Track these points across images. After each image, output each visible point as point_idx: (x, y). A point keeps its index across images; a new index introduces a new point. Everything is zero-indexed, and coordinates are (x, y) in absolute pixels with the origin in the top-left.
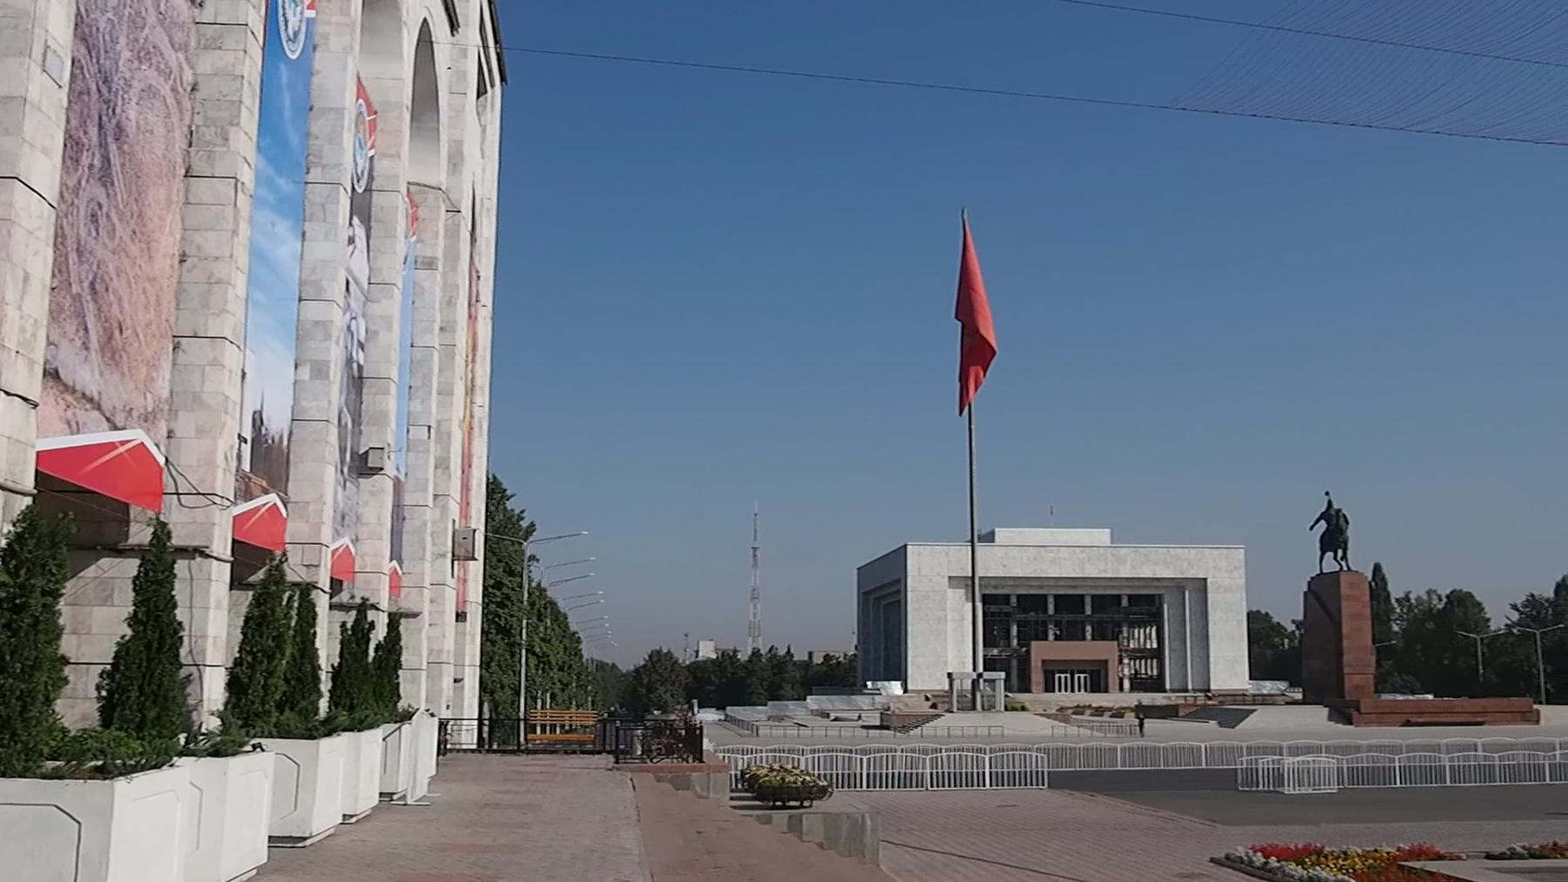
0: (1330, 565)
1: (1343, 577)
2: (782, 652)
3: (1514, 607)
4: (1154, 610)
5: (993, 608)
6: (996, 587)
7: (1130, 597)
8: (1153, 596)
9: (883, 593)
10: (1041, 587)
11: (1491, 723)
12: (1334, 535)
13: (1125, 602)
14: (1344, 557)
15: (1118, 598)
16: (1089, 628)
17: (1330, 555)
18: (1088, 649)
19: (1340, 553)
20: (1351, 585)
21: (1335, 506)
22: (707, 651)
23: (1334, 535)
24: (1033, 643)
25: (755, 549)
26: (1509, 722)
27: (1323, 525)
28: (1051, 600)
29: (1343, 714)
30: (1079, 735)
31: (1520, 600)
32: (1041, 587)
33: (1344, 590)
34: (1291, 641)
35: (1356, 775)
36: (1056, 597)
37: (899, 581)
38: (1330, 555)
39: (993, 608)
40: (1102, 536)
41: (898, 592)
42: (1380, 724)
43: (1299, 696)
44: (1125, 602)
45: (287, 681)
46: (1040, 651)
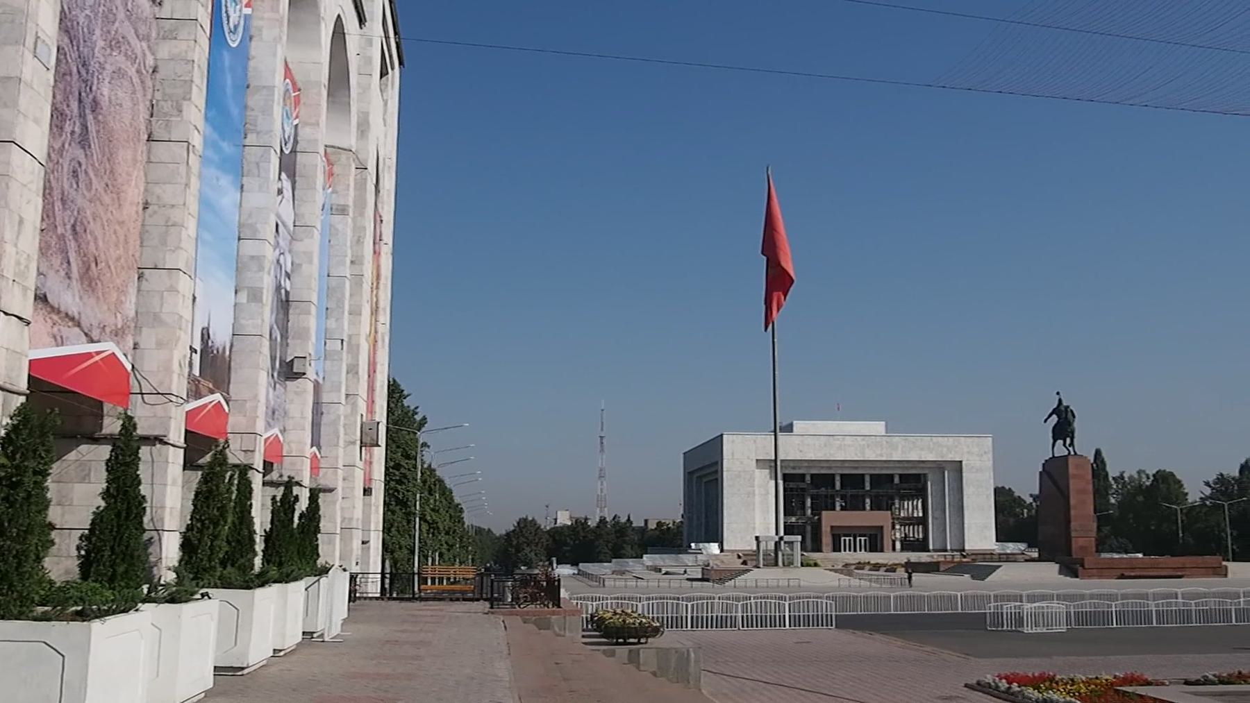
0: (1060, 450)
1: (1071, 460)
2: (623, 520)
3: (1207, 484)
4: (920, 486)
5: (792, 485)
6: (794, 468)
7: (901, 476)
8: (919, 475)
9: (704, 472)
10: (830, 468)
11: (1189, 576)
12: (1063, 427)
13: (897, 480)
14: (1072, 444)
15: (891, 476)
16: (868, 501)
17: (1060, 442)
18: (867, 517)
19: (1068, 440)
20: (1077, 466)
21: (1065, 404)
22: (564, 519)
23: (1063, 427)
24: (824, 513)
25: (602, 437)
26: (1203, 575)
27: (1055, 418)
28: (838, 478)
30: (860, 586)
31: (1212, 478)
32: (830, 468)
33: (1071, 470)
34: (1029, 511)
35: (1081, 618)
36: (842, 476)
37: (716, 463)
38: (1060, 442)
39: (792, 485)
40: (879, 427)
41: (716, 472)
42: (1100, 577)
43: (1036, 555)
44: (897, 480)
45: (229, 542)
46: (829, 519)
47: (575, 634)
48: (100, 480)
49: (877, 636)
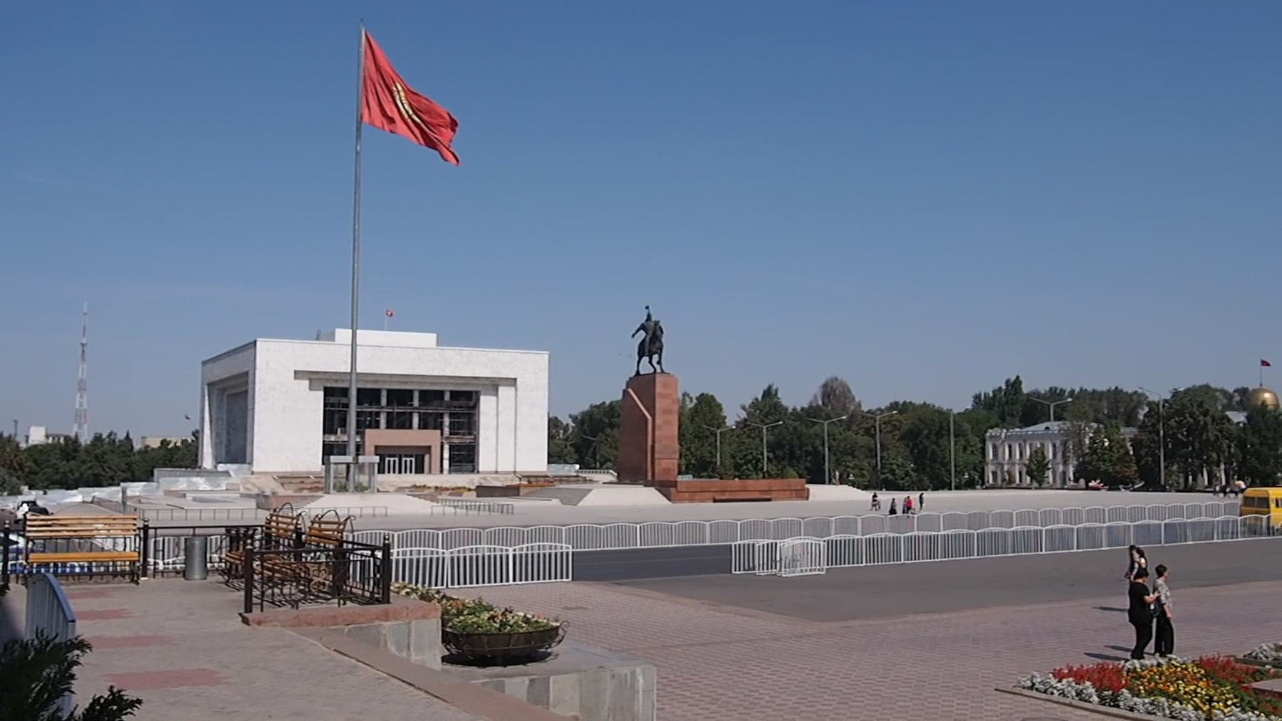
0: (645, 368)
1: (659, 378)
2: (121, 436)
3: (744, 408)
4: (471, 404)
5: (332, 400)
6: (336, 381)
7: (452, 393)
8: (470, 393)
9: (227, 384)
10: (376, 382)
11: (776, 499)
12: (651, 343)
13: (447, 397)
14: (659, 363)
15: (442, 393)
16: (447, 421)
17: (646, 359)
18: (414, 437)
19: (655, 357)
20: (665, 385)
21: (654, 319)
22: (37, 436)
23: (651, 343)
24: (367, 431)
25: (83, 345)
26: (790, 498)
27: (642, 334)
28: (384, 394)
29: (666, 488)
30: (312, 505)
31: (748, 403)
32: (376, 382)
33: (659, 389)
34: (565, 431)
35: (836, 552)
36: (389, 391)
37: (247, 373)
38: (646, 359)
39: (332, 400)
40: (431, 338)
41: (247, 383)
42: (692, 500)
43: (614, 479)
44: (447, 397)
45: (845, 439)
46: (376, 437)
47: (428, 649)
48: (78, 601)
49: (623, 588)
